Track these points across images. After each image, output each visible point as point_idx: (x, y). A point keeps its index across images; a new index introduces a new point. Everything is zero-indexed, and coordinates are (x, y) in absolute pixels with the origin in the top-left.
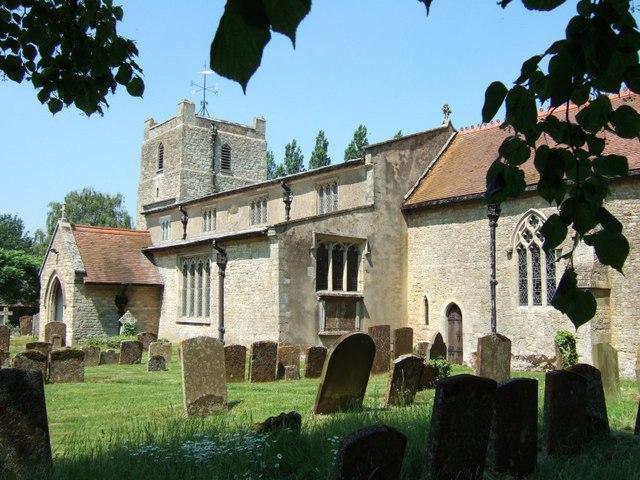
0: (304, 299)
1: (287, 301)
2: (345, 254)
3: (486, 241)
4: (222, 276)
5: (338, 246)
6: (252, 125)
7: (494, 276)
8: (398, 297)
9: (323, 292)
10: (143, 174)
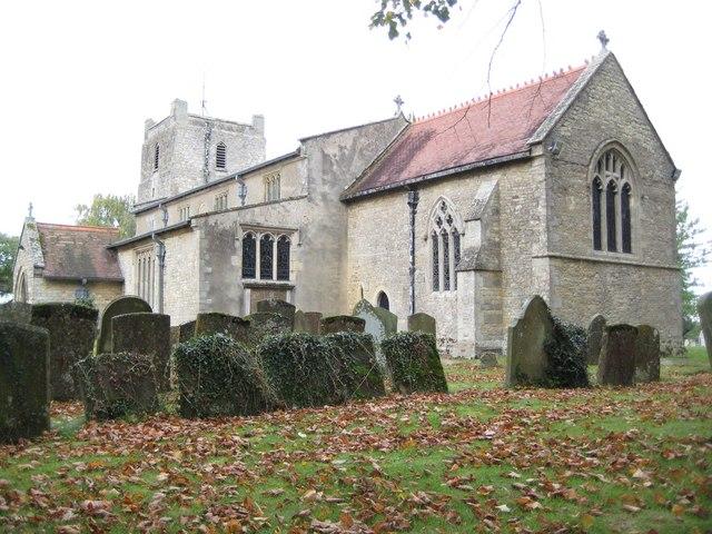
0: (228, 287)
1: (208, 289)
2: (275, 245)
3: (407, 228)
4: (162, 267)
5: (267, 237)
6: (249, 122)
7: (413, 263)
8: (337, 287)
9: (252, 281)
10: (142, 174)
